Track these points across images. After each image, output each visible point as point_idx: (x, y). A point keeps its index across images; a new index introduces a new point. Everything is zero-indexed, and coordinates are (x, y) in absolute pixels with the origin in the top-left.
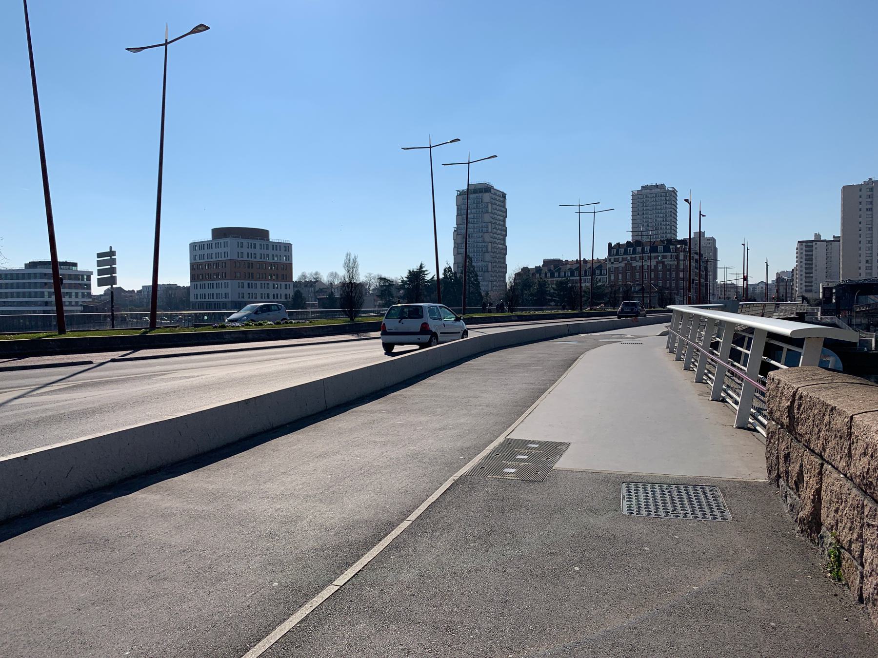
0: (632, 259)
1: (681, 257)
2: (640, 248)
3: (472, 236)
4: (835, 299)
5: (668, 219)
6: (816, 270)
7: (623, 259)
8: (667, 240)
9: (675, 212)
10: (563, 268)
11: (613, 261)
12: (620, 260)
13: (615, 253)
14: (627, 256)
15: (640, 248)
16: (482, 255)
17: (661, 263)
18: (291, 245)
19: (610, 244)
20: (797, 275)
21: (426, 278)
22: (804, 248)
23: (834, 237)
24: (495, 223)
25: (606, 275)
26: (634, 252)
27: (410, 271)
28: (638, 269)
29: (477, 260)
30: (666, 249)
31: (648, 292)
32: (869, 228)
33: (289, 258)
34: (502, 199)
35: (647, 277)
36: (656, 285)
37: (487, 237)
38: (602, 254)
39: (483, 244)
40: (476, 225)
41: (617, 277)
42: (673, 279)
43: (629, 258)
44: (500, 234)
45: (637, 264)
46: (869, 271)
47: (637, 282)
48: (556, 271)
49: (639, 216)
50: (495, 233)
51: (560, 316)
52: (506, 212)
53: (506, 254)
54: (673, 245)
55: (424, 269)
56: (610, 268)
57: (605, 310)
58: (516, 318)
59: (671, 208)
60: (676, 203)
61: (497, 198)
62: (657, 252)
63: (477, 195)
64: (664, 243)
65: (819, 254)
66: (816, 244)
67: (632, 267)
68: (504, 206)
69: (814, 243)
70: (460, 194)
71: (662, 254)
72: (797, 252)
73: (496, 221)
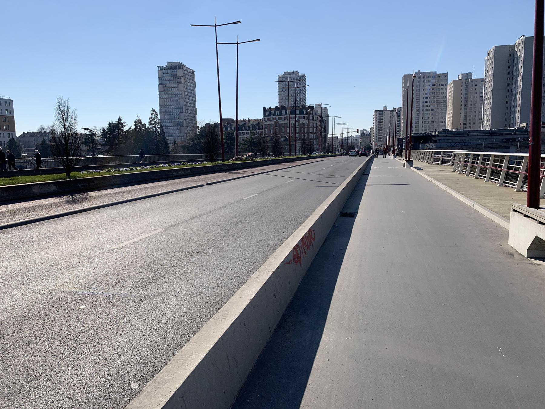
1: (311, 118)
2: (284, 111)
3: (170, 101)
4: (405, 146)
5: (300, 94)
6: (384, 129)
7: (273, 119)
8: (302, 106)
9: (304, 90)
11: (266, 119)
12: (272, 119)
13: (268, 114)
14: (276, 117)
15: (284, 111)
16: (178, 114)
17: (298, 122)
18: (206, 123)
19: (264, 108)
20: (374, 131)
21: (124, 129)
22: (378, 115)
23: (393, 109)
24: (187, 92)
26: (280, 114)
27: (110, 123)
28: (283, 126)
30: (301, 112)
32: (418, 102)
33: (11, 111)
34: (191, 75)
37: (182, 102)
38: (259, 116)
39: (179, 106)
41: (269, 131)
43: (277, 118)
44: (192, 100)
46: (417, 129)
47: (282, 135)
48: (229, 126)
49: (283, 92)
51: (182, 173)
52: (195, 84)
53: (197, 114)
54: (305, 109)
55: (122, 122)
56: (265, 125)
57: (253, 160)
58: (54, 188)
61: (189, 74)
63: (173, 70)
64: (300, 108)
65: (386, 117)
66: (385, 112)
68: (193, 80)
69: (383, 112)
70: (161, 70)
71: (299, 115)
73: (188, 90)
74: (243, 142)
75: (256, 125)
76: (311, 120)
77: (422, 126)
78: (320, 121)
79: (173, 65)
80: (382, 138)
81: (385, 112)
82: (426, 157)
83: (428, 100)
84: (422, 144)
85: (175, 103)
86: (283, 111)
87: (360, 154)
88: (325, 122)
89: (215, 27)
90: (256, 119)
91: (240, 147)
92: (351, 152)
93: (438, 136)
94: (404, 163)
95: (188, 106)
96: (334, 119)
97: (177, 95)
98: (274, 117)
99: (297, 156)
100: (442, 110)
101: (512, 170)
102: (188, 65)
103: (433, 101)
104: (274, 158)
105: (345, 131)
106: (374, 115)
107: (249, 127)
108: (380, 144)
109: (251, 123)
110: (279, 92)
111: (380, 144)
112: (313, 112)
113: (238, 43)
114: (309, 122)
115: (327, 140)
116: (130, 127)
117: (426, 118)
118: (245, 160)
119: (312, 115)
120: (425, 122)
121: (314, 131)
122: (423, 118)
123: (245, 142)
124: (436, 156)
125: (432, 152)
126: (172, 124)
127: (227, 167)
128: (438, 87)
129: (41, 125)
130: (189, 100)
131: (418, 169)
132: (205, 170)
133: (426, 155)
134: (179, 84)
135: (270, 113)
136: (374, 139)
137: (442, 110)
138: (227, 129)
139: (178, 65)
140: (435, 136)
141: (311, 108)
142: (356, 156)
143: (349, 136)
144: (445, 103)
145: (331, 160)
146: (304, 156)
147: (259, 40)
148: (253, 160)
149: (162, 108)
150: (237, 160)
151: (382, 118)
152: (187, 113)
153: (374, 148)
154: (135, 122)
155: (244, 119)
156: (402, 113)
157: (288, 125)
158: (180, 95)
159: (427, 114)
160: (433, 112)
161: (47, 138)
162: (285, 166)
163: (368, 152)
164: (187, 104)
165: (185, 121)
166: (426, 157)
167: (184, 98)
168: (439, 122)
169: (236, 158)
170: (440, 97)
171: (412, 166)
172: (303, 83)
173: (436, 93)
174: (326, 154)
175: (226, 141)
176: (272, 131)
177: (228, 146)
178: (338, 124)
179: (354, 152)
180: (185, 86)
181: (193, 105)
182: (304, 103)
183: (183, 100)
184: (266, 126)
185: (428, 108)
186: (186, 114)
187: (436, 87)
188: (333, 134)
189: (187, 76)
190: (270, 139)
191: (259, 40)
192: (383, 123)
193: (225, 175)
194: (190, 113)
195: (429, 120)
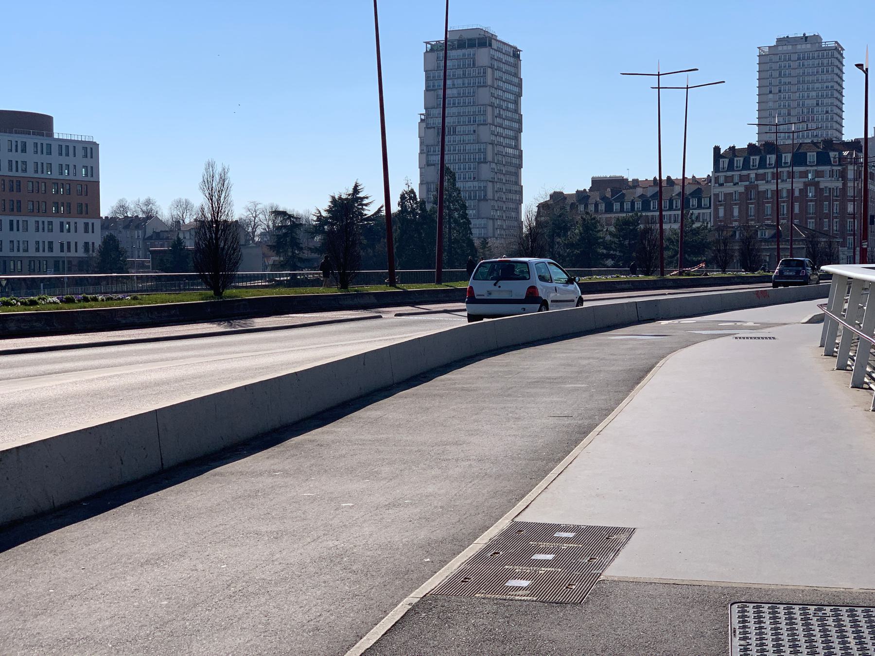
3: (455, 132)
5: (825, 101)
8: (825, 141)
9: (839, 88)
10: (630, 195)
11: (722, 180)
12: (736, 179)
13: (726, 165)
19: (717, 149)
24: (500, 107)
25: (710, 207)
27: (333, 198)
28: (769, 196)
30: (823, 159)
33: (93, 170)
34: (512, 60)
35: (785, 212)
36: (804, 228)
37: (485, 133)
39: (477, 146)
43: (753, 176)
48: (616, 200)
49: (771, 96)
50: (500, 126)
52: (520, 85)
54: (834, 150)
55: (361, 195)
56: (716, 195)
59: (832, 80)
60: (842, 63)
61: (505, 58)
63: (464, 51)
67: (759, 192)
70: (432, 50)
71: (815, 168)
79: (466, 36)
86: (770, 156)
89: (658, 76)
97: (472, 117)
102: (505, 35)
107: (671, 201)
113: (689, 87)
114: (845, 185)
116: (379, 207)
118: (694, 275)
127: (672, 282)
129: (121, 198)
135: (731, 163)
139: (478, 36)
147: (724, 82)
148: (707, 275)
149: (432, 153)
152: (496, 164)
154: (401, 198)
158: (482, 117)
161: (140, 232)
165: (490, 184)
167: (490, 124)
172: (835, 69)
175: (620, 241)
176: (736, 212)
180: (493, 90)
183: (490, 128)
184: (721, 198)
186: (493, 165)
189: (502, 65)
191: (724, 82)
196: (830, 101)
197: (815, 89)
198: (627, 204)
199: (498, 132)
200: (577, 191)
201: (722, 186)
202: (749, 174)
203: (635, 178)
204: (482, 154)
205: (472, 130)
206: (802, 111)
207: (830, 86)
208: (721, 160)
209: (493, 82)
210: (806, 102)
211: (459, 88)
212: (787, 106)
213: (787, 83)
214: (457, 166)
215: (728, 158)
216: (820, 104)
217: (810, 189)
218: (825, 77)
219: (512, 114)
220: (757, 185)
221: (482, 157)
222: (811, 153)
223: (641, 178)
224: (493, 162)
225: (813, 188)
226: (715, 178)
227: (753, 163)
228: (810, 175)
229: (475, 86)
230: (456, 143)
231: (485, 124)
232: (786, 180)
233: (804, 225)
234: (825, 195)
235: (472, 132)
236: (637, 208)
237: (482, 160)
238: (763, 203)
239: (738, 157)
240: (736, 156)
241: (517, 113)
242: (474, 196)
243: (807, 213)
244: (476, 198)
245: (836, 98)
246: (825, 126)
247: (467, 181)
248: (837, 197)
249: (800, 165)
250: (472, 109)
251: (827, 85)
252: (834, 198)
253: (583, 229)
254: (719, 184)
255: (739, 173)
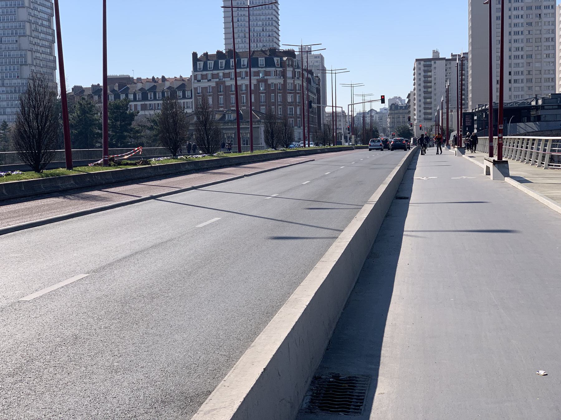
0: (225, 75)
1: (289, 74)
4: (477, 129)
5: (268, 28)
6: (435, 95)
10: (133, 88)
11: (199, 77)
12: (209, 77)
13: (202, 67)
18: (75, 87)
19: (195, 55)
22: (422, 68)
23: (452, 55)
24: (36, 23)
25: (191, 98)
29: (11, 77)
30: (269, 63)
31: (248, 122)
35: (245, 101)
36: (258, 112)
37: (24, 43)
39: (19, 53)
40: (6, 25)
42: (279, 103)
43: (221, 74)
45: (230, 82)
48: (122, 92)
50: (37, 38)
54: (277, 56)
56: (196, 89)
59: (272, 14)
60: (278, 13)
62: (258, 67)
65: (438, 72)
66: (435, 63)
67: (226, 87)
69: (433, 62)
71: (264, 69)
72: (415, 73)
74: (149, 124)
75: (177, 88)
76: (290, 78)
77: (510, 89)
78: (309, 81)
80: (431, 114)
81: (437, 61)
82: (522, 150)
83: (520, 37)
84: (512, 124)
85: (10, 46)
87: (392, 145)
88: (319, 83)
90: (178, 77)
91: (142, 134)
92: (373, 141)
93: (542, 107)
94: (488, 168)
95: (37, 51)
96: (334, 75)
98: (215, 72)
99: (256, 153)
100: (548, 56)
101: (556, 152)
103: (529, 39)
104: (200, 157)
105: (357, 99)
106: (415, 68)
108: (428, 124)
109: (167, 84)
110: (224, 23)
111: (428, 124)
112: (292, 61)
114: (285, 81)
115: (325, 117)
117: (517, 73)
119: (291, 69)
120: (516, 81)
121: (296, 100)
122: (510, 73)
123: (152, 124)
124: (554, 151)
125: (547, 141)
126: (4, 89)
127: (72, 182)
128: (539, 12)
130: (40, 40)
131: (521, 180)
132: (6, 194)
133: (522, 147)
134: (18, 7)
136: (415, 116)
137: (548, 56)
138: (117, 96)
140: (537, 107)
141: (290, 54)
142: (382, 150)
143: (367, 109)
144: (553, 43)
145: (327, 160)
146: (271, 151)
150: (106, 163)
151: (429, 74)
152: (35, 66)
153: (416, 133)
155: (153, 78)
156: (470, 64)
157: (233, 89)
158: (22, 30)
159: (517, 65)
160: (529, 60)
162: (222, 176)
163: (406, 141)
164: (36, 47)
166: (522, 150)
168: (543, 80)
169: (104, 160)
170: (543, 31)
171: (506, 174)
172: (274, 22)
173: (533, 24)
174: (321, 147)
175: (112, 123)
177: (116, 132)
178: (344, 85)
179: (379, 141)
180: (30, 11)
181: (48, 50)
182: (277, 46)
185: (520, 53)
187: (535, 12)
188: (334, 105)
190: (220, 117)
192: (432, 84)
193: (65, 204)
194: (41, 65)
195: (522, 77)
196: (271, 28)
197: (261, 20)
198: (139, 95)
199: (35, 43)
200: (93, 86)
201: (199, 82)
202: (218, 73)
203: (139, 77)
204: (23, 59)
205: (15, 40)
206: (257, 46)
207: (270, 18)
208: (198, 63)
209: (30, 5)
210: (256, 28)
211: (3, 8)
212: (243, 31)
213: (243, 15)
214: (4, 67)
215: (203, 61)
216: (265, 30)
217: (261, 85)
218: (267, 12)
219: (46, 29)
220: (224, 81)
221: (24, 60)
222: (261, 58)
223: (143, 77)
224: (33, 65)
225: (264, 83)
226: (195, 76)
227: (221, 65)
228: (261, 75)
229: (15, 7)
230: (3, 50)
231: (25, 36)
232: (245, 78)
233: (258, 110)
234: (272, 88)
235: (15, 42)
236: (139, 98)
237: (24, 63)
238: (230, 95)
239: (210, 60)
240: (209, 60)
241: (51, 28)
242: (18, 90)
243: (260, 102)
244: (20, 91)
245: (275, 26)
246: (268, 45)
247: (12, 79)
248: (280, 90)
249: (254, 67)
250: (14, 24)
251: (269, 17)
252: (278, 91)
253: (80, 113)
254: (197, 81)
255: (211, 72)
